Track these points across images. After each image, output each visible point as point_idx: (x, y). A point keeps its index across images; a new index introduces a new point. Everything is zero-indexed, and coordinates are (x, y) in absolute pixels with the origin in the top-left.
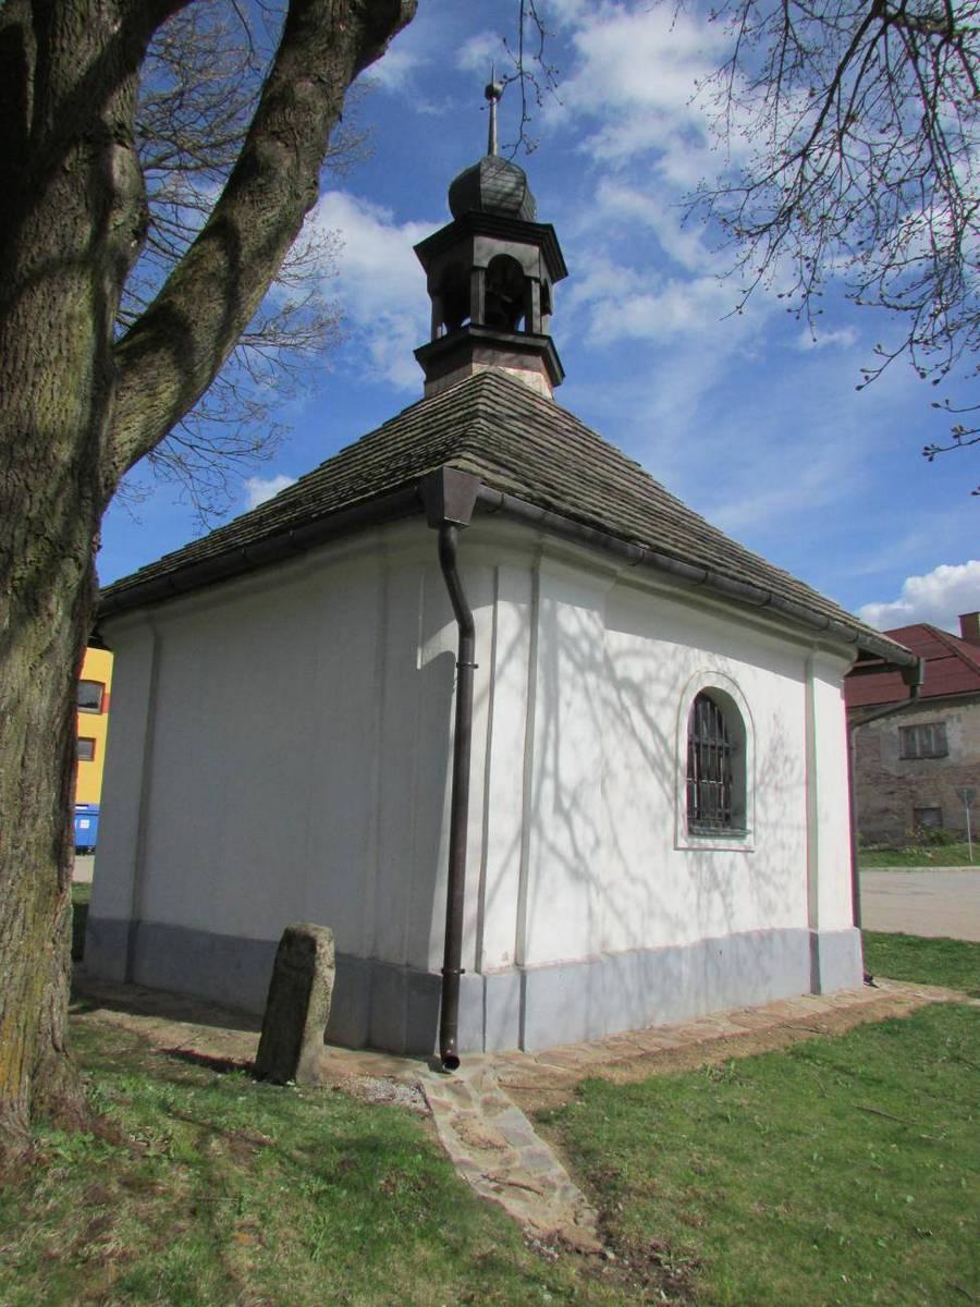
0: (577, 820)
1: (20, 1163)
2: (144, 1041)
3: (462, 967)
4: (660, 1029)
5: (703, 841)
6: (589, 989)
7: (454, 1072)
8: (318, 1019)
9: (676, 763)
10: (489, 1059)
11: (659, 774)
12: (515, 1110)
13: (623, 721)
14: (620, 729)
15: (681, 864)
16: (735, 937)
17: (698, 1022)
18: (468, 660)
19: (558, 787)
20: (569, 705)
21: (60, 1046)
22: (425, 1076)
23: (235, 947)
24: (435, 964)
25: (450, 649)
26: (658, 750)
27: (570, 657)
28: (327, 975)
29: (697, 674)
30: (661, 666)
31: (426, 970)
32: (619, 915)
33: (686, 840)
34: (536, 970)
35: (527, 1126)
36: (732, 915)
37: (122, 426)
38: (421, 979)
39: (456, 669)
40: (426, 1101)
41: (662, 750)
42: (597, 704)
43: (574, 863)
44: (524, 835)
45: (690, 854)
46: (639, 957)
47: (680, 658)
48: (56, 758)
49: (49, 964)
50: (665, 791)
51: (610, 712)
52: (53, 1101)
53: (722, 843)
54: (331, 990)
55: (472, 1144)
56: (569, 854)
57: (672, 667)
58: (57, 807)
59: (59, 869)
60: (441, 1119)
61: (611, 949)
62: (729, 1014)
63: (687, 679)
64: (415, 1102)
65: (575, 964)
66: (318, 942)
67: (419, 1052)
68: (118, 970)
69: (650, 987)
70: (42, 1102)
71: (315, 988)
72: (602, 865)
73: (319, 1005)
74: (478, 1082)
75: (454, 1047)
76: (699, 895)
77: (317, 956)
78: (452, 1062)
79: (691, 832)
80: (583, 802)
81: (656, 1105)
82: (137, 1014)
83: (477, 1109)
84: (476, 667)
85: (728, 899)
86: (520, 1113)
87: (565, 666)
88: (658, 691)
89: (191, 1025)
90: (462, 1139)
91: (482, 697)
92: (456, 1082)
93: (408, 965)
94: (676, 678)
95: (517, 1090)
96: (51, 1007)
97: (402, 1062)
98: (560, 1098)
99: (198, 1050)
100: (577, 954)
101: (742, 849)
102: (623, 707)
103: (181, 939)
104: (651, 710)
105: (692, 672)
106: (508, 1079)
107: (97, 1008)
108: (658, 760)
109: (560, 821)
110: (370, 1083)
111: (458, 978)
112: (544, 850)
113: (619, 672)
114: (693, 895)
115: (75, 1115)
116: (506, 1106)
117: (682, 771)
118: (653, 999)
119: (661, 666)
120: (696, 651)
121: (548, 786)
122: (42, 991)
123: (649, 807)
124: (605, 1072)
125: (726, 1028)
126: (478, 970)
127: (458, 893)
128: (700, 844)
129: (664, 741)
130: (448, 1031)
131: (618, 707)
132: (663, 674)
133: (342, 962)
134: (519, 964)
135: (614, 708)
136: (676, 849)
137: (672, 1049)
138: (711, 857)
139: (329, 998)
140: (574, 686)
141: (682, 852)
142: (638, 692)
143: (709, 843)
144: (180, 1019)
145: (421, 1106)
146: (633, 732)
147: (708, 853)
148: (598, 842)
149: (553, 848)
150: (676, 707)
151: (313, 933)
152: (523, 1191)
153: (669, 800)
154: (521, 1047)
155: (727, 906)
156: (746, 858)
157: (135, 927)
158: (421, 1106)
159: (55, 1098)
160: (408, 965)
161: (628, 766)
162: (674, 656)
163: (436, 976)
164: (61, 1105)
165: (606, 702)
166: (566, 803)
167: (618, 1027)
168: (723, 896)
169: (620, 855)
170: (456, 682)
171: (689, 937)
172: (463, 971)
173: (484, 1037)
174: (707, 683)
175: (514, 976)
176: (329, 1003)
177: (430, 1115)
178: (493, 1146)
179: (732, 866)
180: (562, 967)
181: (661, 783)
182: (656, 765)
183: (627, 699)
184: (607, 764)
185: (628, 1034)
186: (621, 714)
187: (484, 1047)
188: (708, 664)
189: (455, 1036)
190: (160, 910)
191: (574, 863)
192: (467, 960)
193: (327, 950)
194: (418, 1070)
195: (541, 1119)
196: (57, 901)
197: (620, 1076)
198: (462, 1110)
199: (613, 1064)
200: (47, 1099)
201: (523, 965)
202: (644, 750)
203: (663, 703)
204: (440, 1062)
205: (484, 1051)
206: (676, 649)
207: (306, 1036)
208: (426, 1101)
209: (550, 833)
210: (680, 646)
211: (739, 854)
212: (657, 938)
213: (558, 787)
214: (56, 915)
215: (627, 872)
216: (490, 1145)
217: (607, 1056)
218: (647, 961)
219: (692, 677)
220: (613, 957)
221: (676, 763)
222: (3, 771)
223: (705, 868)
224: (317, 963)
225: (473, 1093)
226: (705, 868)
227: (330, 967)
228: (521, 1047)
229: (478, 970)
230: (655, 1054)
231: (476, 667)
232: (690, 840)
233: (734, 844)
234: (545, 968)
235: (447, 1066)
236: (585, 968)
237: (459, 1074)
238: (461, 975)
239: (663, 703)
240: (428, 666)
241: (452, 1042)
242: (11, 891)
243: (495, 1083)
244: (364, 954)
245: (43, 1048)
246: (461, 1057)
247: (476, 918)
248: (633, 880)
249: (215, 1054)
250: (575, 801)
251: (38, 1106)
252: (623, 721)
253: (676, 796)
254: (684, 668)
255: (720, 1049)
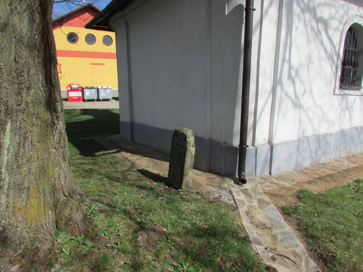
0: (297, 82)
1: (46, 253)
2: (133, 165)
3: (247, 145)
4: (322, 164)
5: (345, 91)
6: (298, 149)
7: (245, 185)
8: (189, 167)
9: (338, 56)
10: (258, 179)
11: (331, 62)
12: (272, 206)
13: (318, 38)
14: (317, 42)
15: (336, 100)
16: (351, 129)
17: (336, 161)
18: (250, 6)
19: (290, 67)
20: (297, 29)
21: (67, 194)
22: (233, 186)
23: (161, 132)
24: (236, 142)
25: (242, 3)
26: (332, 51)
27: (298, 5)
28: (192, 150)
29: (352, 16)
30: (337, 11)
31: (232, 145)
32: (310, 121)
33: (339, 91)
34: (277, 145)
35: (278, 216)
36: (352, 120)
37: (288, 211)
38: (230, 149)
39: (244, 12)
40: (234, 200)
41: (333, 51)
42: (309, 29)
43: (295, 100)
44: (274, 91)
45: (339, 96)
46: (317, 137)
47: (346, 8)
48: (39, 57)
49: (55, 159)
50: (332, 69)
51: (313, 33)
52: (66, 219)
53: (352, 92)
54: (194, 155)
55: (257, 226)
56: (293, 97)
57: (341, 12)
58: (44, 83)
59: (51, 114)
60: (242, 210)
61: (306, 135)
62: (346, 157)
63: (347, 18)
64: (229, 200)
65: (294, 141)
66: (187, 137)
67: (230, 175)
68: (129, 139)
69: (320, 148)
70: (61, 220)
71: (187, 155)
72: (306, 101)
73: (189, 161)
74: (254, 189)
75: (244, 176)
76: (341, 113)
77: (187, 142)
78: (244, 182)
79: (341, 87)
80: (300, 74)
81: (335, 206)
82: (133, 154)
83: (255, 203)
84: (254, 10)
85: (351, 114)
86: (275, 208)
87: (296, 9)
88: (334, 24)
89: (149, 158)
90: (252, 223)
91: (256, 27)
92: (245, 189)
93: (224, 143)
94: (343, 17)
95: (271, 195)
96: (59, 178)
97: (223, 179)
98: (292, 201)
99: (150, 170)
100: (294, 137)
101: (360, 94)
102: (319, 31)
103: (145, 128)
104: (330, 33)
105: (350, 15)
106: (267, 189)
107: (122, 151)
108: (331, 55)
109: (290, 82)
110: (211, 189)
111: (246, 148)
112: (283, 94)
113: (319, 14)
114: (339, 112)
115: (76, 225)
116: (268, 203)
117: (340, 60)
118: (320, 152)
119: (337, 11)
120: (352, 5)
121: (286, 66)
122: (53, 172)
123: (325, 77)
124: (307, 186)
125: (347, 164)
126: (253, 145)
127: (245, 115)
128: (344, 93)
129: (334, 47)
130: (242, 169)
131: (317, 31)
132: (337, 16)
133: (198, 140)
134: (270, 143)
135: (315, 31)
136: (334, 94)
137: (331, 174)
138: (347, 97)
139: (193, 158)
140: (299, 20)
141: (336, 96)
142: (325, 24)
143: (347, 92)
144: (146, 156)
145: (232, 202)
146: (322, 43)
147: (346, 96)
148: (305, 91)
149: (286, 94)
150: (341, 31)
151: (185, 132)
152: (285, 259)
153: (334, 74)
154: (270, 173)
155: (351, 116)
156: (360, 98)
157: (132, 124)
158: (232, 202)
159: (67, 218)
160: (224, 143)
161: (319, 59)
162: (343, 7)
163: (236, 148)
164: (70, 221)
165: (312, 29)
166: (293, 74)
167: (307, 163)
168: (350, 112)
169: (312, 96)
170: (244, 19)
171: (335, 129)
172: (248, 146)
173: (256, 170)
174: (355, 21)
175: (268, 147)
176: (193, 160)
177: (237, 208)
178: (266, 228)
179: (354, 100)
180: (287, 143)
181: (331, 66)
182: (330, 58)
183: (321, 27)
184: (310, 57)
185: (311, 167)
186: (318, 34)
187: (256, 174)
188: (357, 12)
189: (244, 171)
190: (141, 118)
191: (295, 100)
192: (249, 142)
193: (191, 140)
194: (229, 183)
195: (286, 212)
196: (52, 130)
197: (314, 189)
198: (250, 204)
199: (309, 183)
200: (63, 218)
201: (272, 143)
202: (326, 51)
203: (336, 29)
204: (238, 180)
205: (256, 176)
206: (344, 4)
207: (185, 173)
208: (234, 200)
209: (286, 88)
210: (346, 3)
211: (358, 96)
212: (323, 130)
213: (290, 67)
214: (54, 136)
215: (314, 104)
216: (264, 227)
217: (306, 178)
218: (320, 139)
219: (350, 17)
220: (307, 138)
221: (338, 56)
222: (2, 64)
223: (344, 101)
224: (187, 145)
225: (253, 195)
226: (344, 101)
227: (193, 146)
228: (270, 173)
229: (253, 145)
230: (324, 177)
231: (254, 10)
232: (340, 91)
233: (357, 92)
234: (280, 144)
235: (241, 183)
236: (297, 142)
237: (246, 186)
238: (247, 148)
239: (336, 29)
240: (231, 13)
241: (243, 173)
242: (20, 128)
243: (261, 191)
244: (207, 137)
245: (58, 196)
246: (247, 178)
247: (253, 125)
248: (317, 107)
249: (155, 171)
250: (297, 73)
251: (60, 222)
252: (318, 38)
253: (336, 72)
254: (346, 13)
255: (350, 174)
